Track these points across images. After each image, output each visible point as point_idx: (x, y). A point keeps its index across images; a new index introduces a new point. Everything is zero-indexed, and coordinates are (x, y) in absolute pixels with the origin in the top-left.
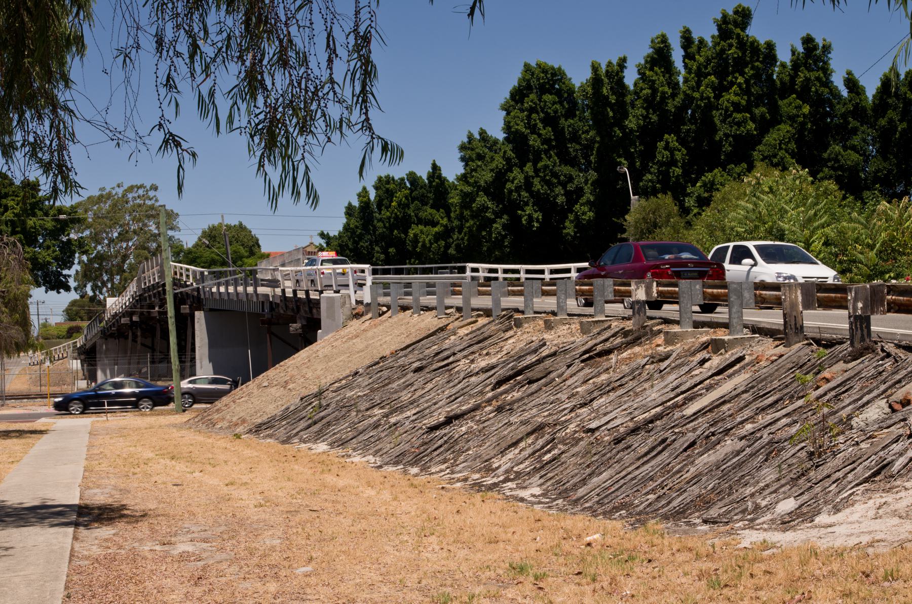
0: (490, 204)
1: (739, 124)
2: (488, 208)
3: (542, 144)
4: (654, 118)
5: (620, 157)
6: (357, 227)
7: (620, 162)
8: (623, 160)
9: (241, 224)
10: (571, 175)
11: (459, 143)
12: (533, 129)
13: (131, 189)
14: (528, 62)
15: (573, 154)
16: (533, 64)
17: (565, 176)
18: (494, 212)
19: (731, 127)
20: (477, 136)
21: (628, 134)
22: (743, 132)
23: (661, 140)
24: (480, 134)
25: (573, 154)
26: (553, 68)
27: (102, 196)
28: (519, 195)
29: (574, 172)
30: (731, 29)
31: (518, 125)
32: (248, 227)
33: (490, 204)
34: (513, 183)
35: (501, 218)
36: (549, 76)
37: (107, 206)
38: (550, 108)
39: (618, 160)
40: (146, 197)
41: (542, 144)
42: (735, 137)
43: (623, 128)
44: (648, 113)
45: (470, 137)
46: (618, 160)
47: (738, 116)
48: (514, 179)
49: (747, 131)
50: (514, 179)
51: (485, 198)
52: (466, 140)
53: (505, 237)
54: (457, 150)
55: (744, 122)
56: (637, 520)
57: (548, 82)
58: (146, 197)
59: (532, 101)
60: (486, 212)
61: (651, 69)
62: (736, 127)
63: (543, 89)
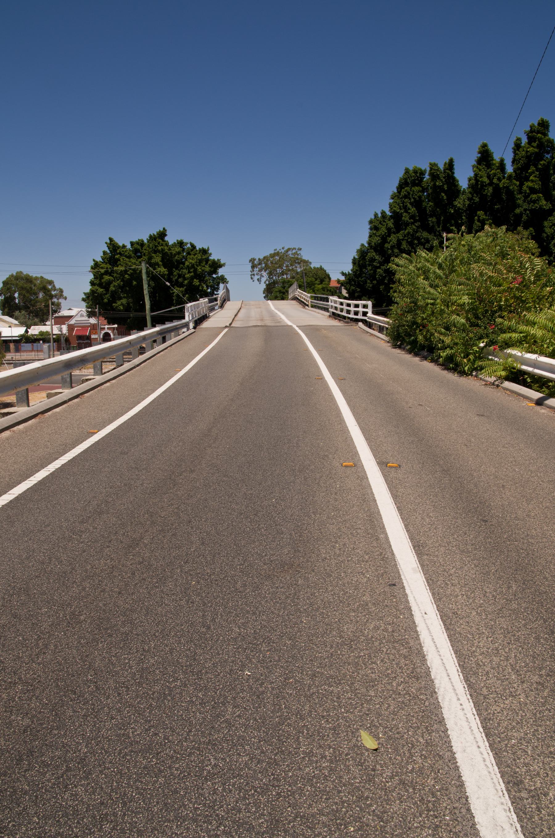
0: (377, 257)
1: (534, 202)
2: (375, 260)
3: (410, 219)
4: (477, 200)
5: (452, 226)
6: (357, 270)
7: (452, 229)
8: (454, 228)
9: (321, 267)
10: (428, 238)
11: (369, 219)
12: (406, 210)
13: (289, 249)
14: (407, 167)
15: (431, 224)
16: (411, 168)
17: (424, 239)
18: (379, 262)
19: (529, 204)
20: (380, 215)
21: (458, 212)
22: (536, 207)
23: (476, 215)
24: (382, 213)
25: (431, 224)
26: (421, 170)
27: (275, 253)
28: (393, 251)
29: (430, 237)
30: (534, 136)
31: (395, 207)
32: (325, 269)
33: (377, 257)
34: (389, 243)
35: (383, 266)
36: (418, 175)
37: (277, 258)
38: (416, 195)
39: (451, 228)
40: (296, 253)
41: (410, 219)
42: (531, 211)
43: (454, 207)
44: (473, 196)
45: (376, 215)
46: (451, 228)
47: (534, 196)
48: (390, 241)
49: (540, 206)
50: (390, 241)
51: (374, 254)
52: (373, 217)
53: (385, 277)
54: (367, 223)
55: (538, 199)
56: (40, 609)
57: (417, 179)
58: (296, 253)
59: (406, 191)
60: (374, 262)
61: (480, 165)
62: (532, 204)
63: (414, 184)
